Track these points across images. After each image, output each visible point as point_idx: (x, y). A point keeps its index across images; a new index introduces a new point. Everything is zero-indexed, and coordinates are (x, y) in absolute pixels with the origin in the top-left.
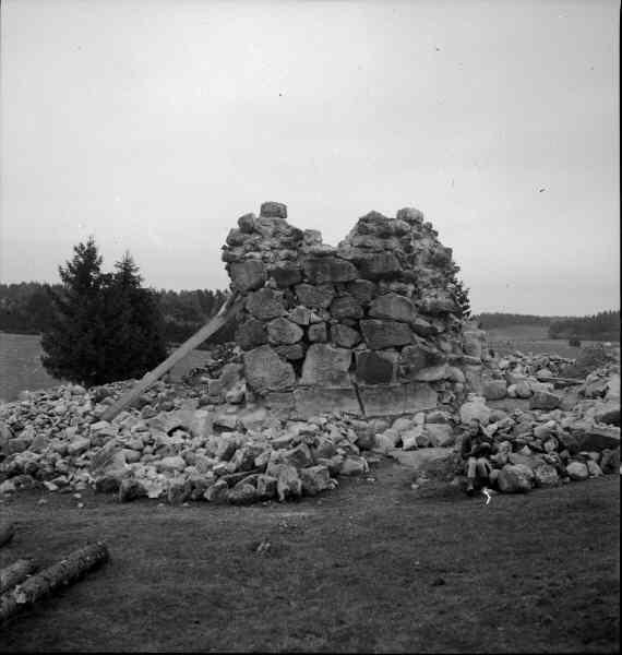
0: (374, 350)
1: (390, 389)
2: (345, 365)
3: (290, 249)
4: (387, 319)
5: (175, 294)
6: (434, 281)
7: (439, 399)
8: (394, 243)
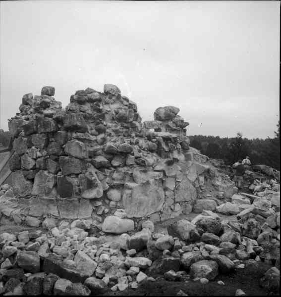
0: (65, 176)
1: (71, 202)
2: (51, 184)
3: (38, 113)
4: (71, 156)
5: (263, 140)
6: (116, 132)
7: (94, 211)
8: (87, 107)
